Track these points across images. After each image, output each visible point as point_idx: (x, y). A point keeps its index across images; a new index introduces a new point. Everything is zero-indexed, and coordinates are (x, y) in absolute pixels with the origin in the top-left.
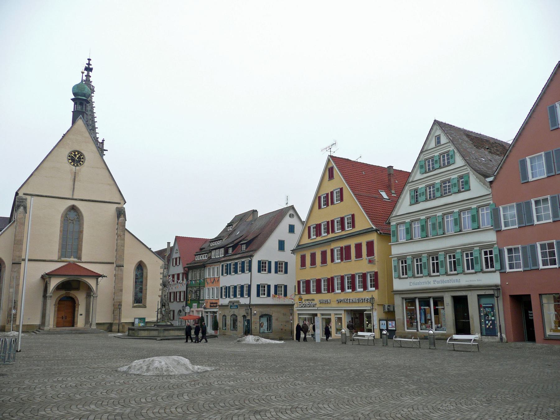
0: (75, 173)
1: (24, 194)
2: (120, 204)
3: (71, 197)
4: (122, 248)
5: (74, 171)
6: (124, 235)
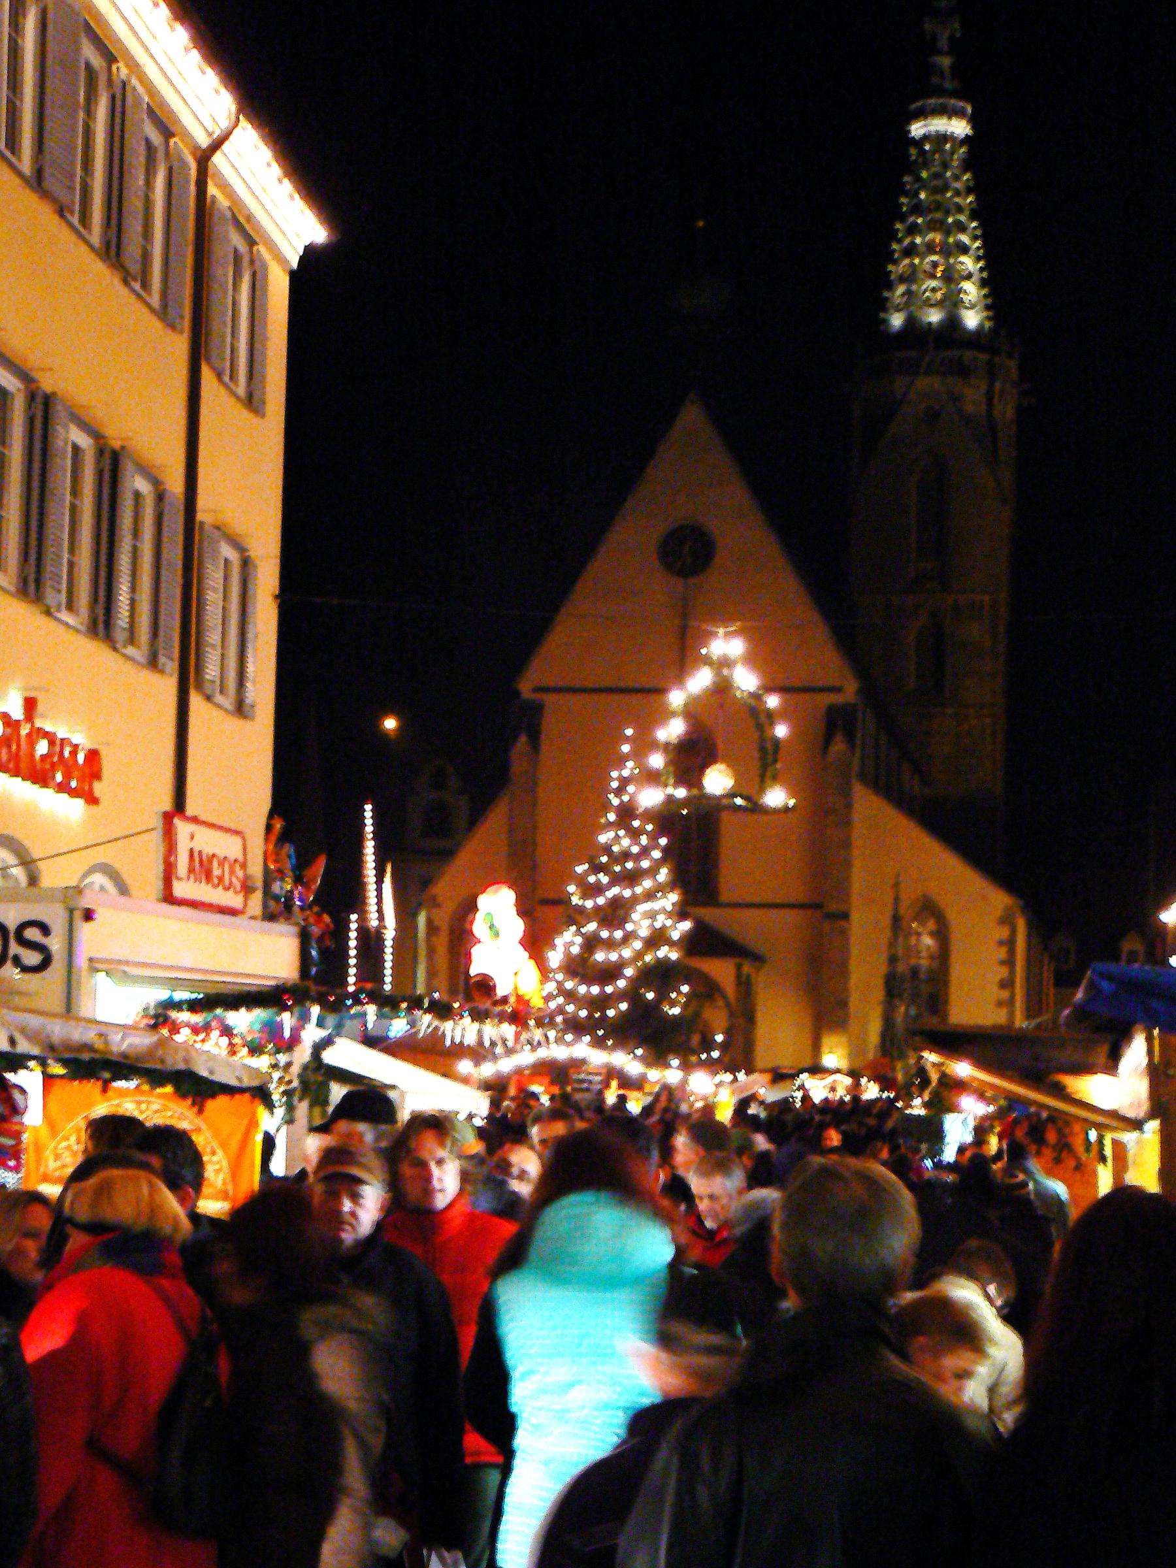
2: (837, 690)
6: (849, 806)
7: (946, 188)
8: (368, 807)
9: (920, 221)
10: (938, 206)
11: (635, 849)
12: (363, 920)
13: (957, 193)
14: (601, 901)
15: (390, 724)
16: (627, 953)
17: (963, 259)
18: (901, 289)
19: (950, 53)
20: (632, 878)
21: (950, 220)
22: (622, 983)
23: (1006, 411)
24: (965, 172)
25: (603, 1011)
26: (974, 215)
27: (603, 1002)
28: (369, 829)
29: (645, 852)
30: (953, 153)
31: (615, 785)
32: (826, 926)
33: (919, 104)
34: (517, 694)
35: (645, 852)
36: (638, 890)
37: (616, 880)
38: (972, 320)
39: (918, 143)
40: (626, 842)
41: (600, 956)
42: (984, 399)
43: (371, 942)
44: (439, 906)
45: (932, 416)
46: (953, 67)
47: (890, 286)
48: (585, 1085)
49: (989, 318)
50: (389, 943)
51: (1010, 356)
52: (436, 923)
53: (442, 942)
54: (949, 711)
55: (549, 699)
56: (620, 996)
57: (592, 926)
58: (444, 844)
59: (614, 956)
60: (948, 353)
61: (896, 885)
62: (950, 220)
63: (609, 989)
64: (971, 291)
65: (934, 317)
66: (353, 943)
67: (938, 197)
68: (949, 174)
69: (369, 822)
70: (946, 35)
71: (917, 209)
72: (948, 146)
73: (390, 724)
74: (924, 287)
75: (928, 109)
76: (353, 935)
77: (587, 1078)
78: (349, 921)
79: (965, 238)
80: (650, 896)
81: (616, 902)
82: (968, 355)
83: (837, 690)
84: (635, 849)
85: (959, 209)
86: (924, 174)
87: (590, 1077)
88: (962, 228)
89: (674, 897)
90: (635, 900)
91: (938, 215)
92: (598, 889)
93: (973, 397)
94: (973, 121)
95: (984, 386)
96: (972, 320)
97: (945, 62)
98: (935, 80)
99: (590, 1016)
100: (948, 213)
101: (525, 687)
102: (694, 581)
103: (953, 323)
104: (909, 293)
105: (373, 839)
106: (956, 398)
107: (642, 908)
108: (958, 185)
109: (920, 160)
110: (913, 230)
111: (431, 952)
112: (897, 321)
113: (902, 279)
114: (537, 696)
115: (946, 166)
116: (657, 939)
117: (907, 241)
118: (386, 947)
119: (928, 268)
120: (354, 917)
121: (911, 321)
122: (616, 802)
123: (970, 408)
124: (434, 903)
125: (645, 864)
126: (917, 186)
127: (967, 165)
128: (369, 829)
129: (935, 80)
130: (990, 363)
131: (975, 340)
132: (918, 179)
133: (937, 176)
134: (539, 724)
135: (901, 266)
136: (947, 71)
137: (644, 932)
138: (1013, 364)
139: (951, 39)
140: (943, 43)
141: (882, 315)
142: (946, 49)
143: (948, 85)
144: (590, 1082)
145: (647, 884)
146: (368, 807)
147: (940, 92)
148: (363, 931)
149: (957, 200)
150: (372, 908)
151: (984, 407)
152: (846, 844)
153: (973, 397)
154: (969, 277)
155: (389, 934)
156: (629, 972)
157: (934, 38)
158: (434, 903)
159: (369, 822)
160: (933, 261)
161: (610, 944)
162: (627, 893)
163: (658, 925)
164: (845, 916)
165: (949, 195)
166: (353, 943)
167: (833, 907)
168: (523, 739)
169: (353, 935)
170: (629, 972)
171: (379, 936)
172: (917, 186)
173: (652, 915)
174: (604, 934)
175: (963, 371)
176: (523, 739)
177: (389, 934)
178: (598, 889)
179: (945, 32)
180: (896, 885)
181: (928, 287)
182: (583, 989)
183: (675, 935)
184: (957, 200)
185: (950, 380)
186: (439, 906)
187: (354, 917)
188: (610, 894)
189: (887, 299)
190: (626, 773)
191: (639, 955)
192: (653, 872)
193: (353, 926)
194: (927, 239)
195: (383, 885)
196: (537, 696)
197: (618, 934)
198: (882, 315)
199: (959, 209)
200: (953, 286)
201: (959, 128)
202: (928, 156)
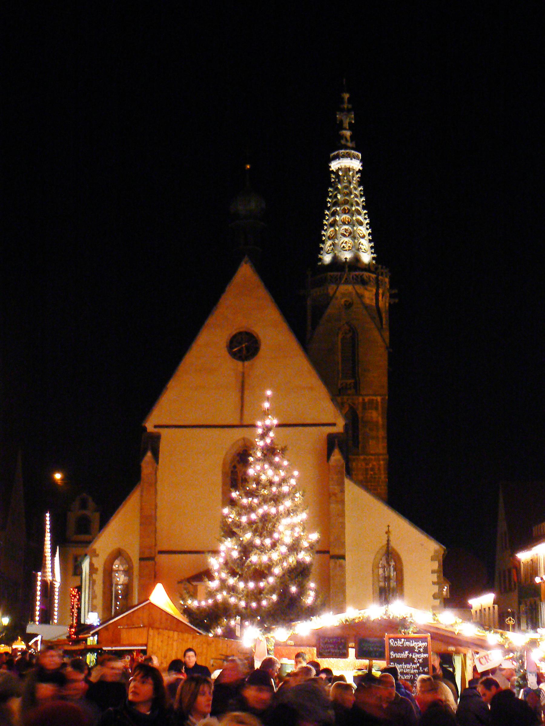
0: (243, 373)
1: (156, 427)
2: (334, 425)
3: (236, 422)
4: (340, 520)
5: (241, 370)
6: (342, 491)
7: (351, 193)
8: (48, 515)
9: (338, 209)
10: (346, 202)
11: (276, 479)
12: (43, 576)
13: (356, 196)
14: (253, 516)
15: (58, 476)
16: (275, 556)
17: (360, 228)
18: (330, 242)
19: (350, 129)
20: (276, 499)
21: (354, 209)
22: (271, 580)
23: (384, 303)
24: (359, 186)
25: (259, 601)
26: (364, 208)
27: (257, 595)
28: (48, 527)
29: (284, 480)
30: (353, 177)
31: (260, 431)
32: (332, 563)
33: (336, 153)
34: (145, 429)
35: (284, 480)
36: (281, 508)
37: (265, 500)
38: (366, 258)
39: (336, 173)
40: (270, 472)
41: (254, 558)
42: (374, 297)
43: (48, 589)
44: (97, 556)
45: (349, 305)
46: (351, 137)
47: (323, 242)
48: (405, 654)
49: (374, 258)
50: (57, 590)
51: (386, 276)
52: (96, 566)
53: (99, 577)
54: (362, 457)
55: (164, 432)
56: (273, 590)
57: (248, 536)
58: (86, 537)
59: (265, 558)
60: (357, 273)
61: (388, 532)
62: (354, 209)
63: (262, 584)
64: (365, 244)
65: (347, 256)
66: (39, 588)
67: (347, 198)
68: (352, 187)
69: (48, 523)
70: (348, 121)
71: (336, 204)
72: (351, 173)
73: (58, 476)
74: (342, 241)
75: (341, 155)
76: (39, 583)
77: (407, 644)
78: (37, 576)
79: (360, 218)
80: (288, 513)
81: (265, 518)
82: (366, 274)
83: (334, 425)
84: (276, 479)
85: (358, 204)
86: (339, 186)
87: (413, 644)
88: (359, 213)
89: (303, 516)
90: (278, 517)
91: (347, 207)
92: (251, 509)
93: (369, 295)
94: (363, 161)
95: (374, 291)
96: (366, 258)
97: (348, 133)
98: (343, 142)
99: (247, 607)
100: (352, 205)
101: (149, 426)
102: (247, 363)
103: (357, 259)
104: (334, 244)
105: (50, 532)
106: (360, 296)
107: (285, 521)
108: (357, 192)
109: (337, 180)
110: (334, 214)
111: (92, 582)
112: (327, 259)
113: (329, 238)
114: (156, 430)
115: (350, 183)
116: (294, 548)
117: (332, 219)
118: (55, 595)
119: (343, 232)
120: (39, 574)
121: (335, 258)
122: (261, 443)
123: (367, 301)
124: (95, 554)
125: (285, 489)
126: (335, 193)
127: (360, 183)
128: (48, 527)
129: (343, 142)
130: (377, 278)
131: (368, 268)
132: (337, 189)
133: (346, 187)
134: (158, 447)
135: (329, 232)
136: (349, 138)
137: (288, 540)
138: (387, 280)
139: (350, 123)
140: (346, 125)
141: (320, 256)
142: (348, 128)
143: (349, 144)
144: (411, 650)
145: (288, 503)
146: (48, 515)
147: (346, 148)
148: (44, 583)
149: (356, 199)
150: (49, 570)
151: (374, 301)
152: (342, 514)
153: (369, 295)
154: (363, 237)
155: (57, 585)
156: (277, 570)
157: (341, 122)
158: (95, 554)
159: (48, 523)
160: (346, 229)
161: (262, 549)
162: (273, 510)
163: (296, 535)
164: (343, 557)
165: (352, 196)
166: (39, 588)
167: (335, 551)
168: (149, 454)
169: (39, 583)
170: (277, 570)
171: (52, 584)
172: (335, 193)
173: (292, 527)
174: (258, 541)
175: (364, 282)
176: (149, 454)
177: (57, 585)
178: (251, 509)
179: (348, 119)
180: (388, 532)
181: (343, 241)
182: (241, 585)
183: (305, 544)
184: (356, 199)
185: (357, 287)
186: (97, 556)
187: (39, 574)
188: (260, 511)
189: (322, 249)
190: (268, 422)
191: (284, 558)
192: (291, 495)
193: (39, 578)
194: (342, 217)
195: (55, 558)
196: (156, 430)
197: (268, 542)
198: (320, 256)
199: (358, 204)
200: (356, 241)
201: (356, 165)
202: (341, 178)
